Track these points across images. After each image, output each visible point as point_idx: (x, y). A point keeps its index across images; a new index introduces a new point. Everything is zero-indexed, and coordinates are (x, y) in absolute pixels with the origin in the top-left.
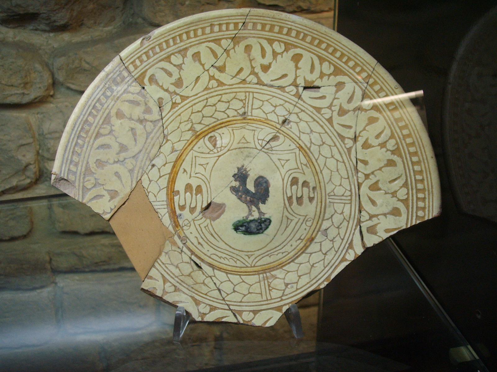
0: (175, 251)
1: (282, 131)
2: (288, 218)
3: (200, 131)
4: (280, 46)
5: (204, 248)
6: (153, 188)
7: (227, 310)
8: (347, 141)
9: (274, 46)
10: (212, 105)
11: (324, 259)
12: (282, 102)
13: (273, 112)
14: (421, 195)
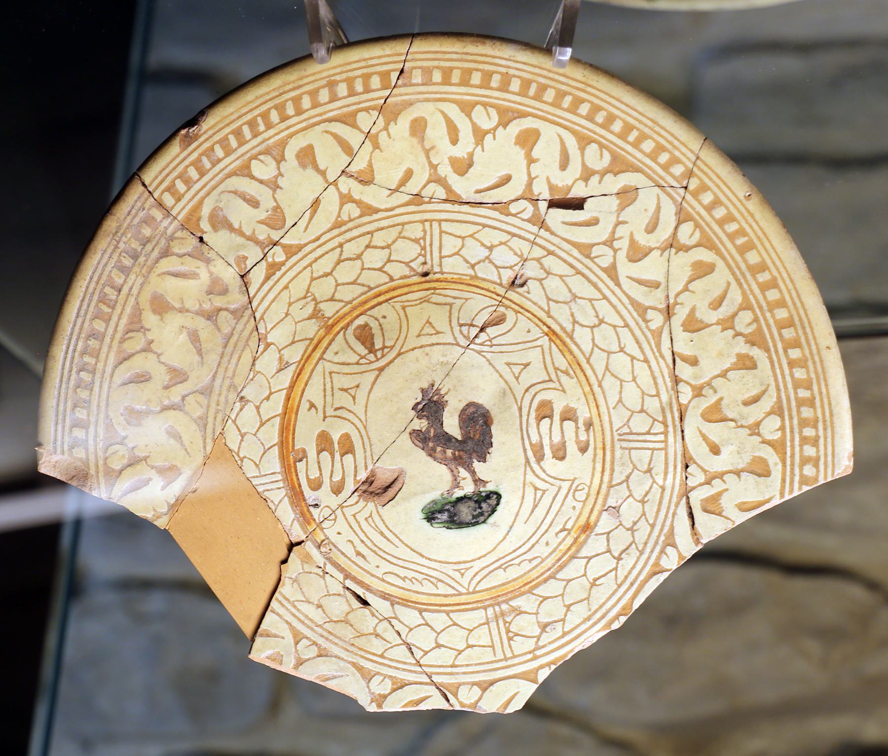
0: (311, 573)
1: (511, 301)
2: (536, 489)
3: (334, 315)
4: (488, 114)
5: (368, 562)
6: (250, 449)
7: (426, 684)
8: (651, 314)
9: (474, 115)
10: (352, 256)
11: (616, 569)
12: (505, 237)
13: (487, 261)
14: (809, 432)
